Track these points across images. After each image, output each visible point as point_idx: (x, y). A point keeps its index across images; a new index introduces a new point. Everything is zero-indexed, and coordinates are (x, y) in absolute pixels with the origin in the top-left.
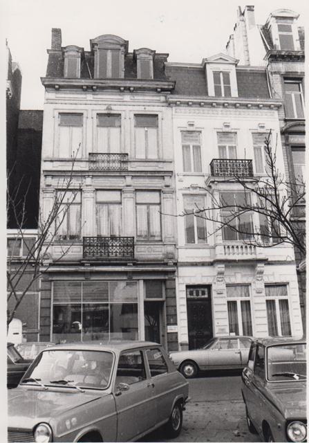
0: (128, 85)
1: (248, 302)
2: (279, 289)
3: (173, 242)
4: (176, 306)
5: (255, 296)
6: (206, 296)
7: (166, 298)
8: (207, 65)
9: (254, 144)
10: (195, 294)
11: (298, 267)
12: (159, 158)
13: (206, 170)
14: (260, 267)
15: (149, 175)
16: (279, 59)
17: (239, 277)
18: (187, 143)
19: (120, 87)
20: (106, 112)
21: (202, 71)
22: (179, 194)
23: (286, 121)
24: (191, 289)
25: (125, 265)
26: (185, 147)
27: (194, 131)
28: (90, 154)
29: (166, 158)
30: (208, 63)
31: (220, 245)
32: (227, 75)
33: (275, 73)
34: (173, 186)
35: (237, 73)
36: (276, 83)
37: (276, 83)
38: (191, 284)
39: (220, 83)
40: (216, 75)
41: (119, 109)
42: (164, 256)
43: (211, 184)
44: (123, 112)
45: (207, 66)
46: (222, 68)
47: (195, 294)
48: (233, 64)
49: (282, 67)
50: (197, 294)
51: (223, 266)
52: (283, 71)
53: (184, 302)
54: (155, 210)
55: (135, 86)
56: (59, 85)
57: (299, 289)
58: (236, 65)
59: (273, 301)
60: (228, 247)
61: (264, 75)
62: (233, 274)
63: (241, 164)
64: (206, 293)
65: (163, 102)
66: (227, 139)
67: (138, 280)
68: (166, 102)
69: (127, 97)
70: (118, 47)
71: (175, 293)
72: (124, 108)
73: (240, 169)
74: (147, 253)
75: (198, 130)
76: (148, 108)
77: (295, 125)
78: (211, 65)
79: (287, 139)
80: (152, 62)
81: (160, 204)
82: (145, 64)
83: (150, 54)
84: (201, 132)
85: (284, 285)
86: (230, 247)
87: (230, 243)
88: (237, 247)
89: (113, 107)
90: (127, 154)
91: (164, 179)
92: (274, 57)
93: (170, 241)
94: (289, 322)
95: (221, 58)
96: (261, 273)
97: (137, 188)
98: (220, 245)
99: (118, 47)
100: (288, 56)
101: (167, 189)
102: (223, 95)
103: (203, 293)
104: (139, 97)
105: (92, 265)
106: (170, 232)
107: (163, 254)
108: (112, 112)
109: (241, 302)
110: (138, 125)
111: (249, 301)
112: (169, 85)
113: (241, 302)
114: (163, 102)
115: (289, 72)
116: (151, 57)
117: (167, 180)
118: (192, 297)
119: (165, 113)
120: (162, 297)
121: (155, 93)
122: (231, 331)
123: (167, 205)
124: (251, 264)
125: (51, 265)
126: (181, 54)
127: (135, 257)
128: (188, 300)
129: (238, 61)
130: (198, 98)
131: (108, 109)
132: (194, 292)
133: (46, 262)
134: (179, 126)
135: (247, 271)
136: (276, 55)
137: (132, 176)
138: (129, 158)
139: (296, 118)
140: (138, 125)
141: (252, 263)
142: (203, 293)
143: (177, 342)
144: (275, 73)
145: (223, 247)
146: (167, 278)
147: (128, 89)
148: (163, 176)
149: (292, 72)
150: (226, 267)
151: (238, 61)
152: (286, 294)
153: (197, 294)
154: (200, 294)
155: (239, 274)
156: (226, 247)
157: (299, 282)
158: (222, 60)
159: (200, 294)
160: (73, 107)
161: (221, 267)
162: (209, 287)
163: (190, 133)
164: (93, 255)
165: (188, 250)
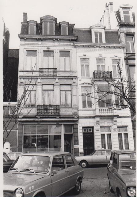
0: (57, 38)
1: (110, 134)
2: (124, 129)
3: (77, 107)
4: (78, 136)
5: (113, 132)
6: (91, 132)
7: (74, 132)
8: (92, 29)
9: (113, 64)
10: (86, 131)
11: (132, 119)
12: (71, 70)
13: (91, 75)
14: (115, 119)
15: (66, 78)
16: (124, 26)
17: (106, 123)
18: (83, 64)
19: (53, 39)
20: (47, 50)
21: (90, 32)
22: (79, 86)
23: (127, 54)
24: (85, 129)
25: (56, 118)
26: (82, 66)
27: (86, 58)
28: (40, 68)
29: (73, 70)
30: (92, 28)
31: (98, 109)
32: (100, 33)
33: (122, 32)
34: (77, 83)
35: (105, 32)
36: (123, 37)
37: (123, 37)
38: (85, 126)
39: (97, 37)
40: (96, 33)
41: (53, 49)
42: (73, 114)
43: (93, 82)
44: (55, 50)
45: (92, 29)
46: (99, 30)
47: (86, 131)
48: (103, 28)
49: (125, 30)
50: (88, 131)
51: (99, 118)
52: (125, 32)
53: (82, 134)
54: (69, 93)
55: (60, 38)
56: (26, 38)
57: (133, 128)
58: (105, 29)
59: (121, 134)
60: (101, 110)
61: (117, 33)
62: (103, 122)
63: (107, 73)
64: (92, 130)
65: (72, 45)
66: (101, 62)
67: (61, 124)
68: (74, 45)
69: (56, 43)
70: (52, 21)
71: (77, 130)
72: (55, 48)
73: (106, 75)
74: (65, 112)
75: (88, 58)
76: (65, 48)
77: (131, 56)
78: (94, 29)
79: (127, 62)
80: (67, 28)
81: (71, 91)
82: (64, 28)
83: (66, 24)
84: (89, 59)
85: (126, 127)
86: (102, 110)
87: (102, 108)
88: (105, 110)
89: (50, 48)
90: (56, 69)
91: (73, 79)
92: (122, 25)
93: (75, 107)
94: (128, 143)
95: (98, 26)
96: (116, 121)
97: (61, 84)
98: (98, 109)
99: (52, 21)
100: (128, 25)
101: (74, 84)
102: (99, 42)
103: (90, 130)
104: (62, 43)
105: (41, 118)
106: (75, 103)
107: (72, 113)
108: (50, 50)
109: (107, 134)
110: (61, 56)
111: (110, 134)
112: (75, 38)
113: (107, 134)
114: (72, 45)
115: (128, 32)
116: (67, 25)
117: (74, 80)
118: (85, 132)
119: (73, 50)
120: (72, 132)
121: (69, 41)
122: (102, 147)
123: (74, 91)
124: (111, 117)
125: (22, 118)
126: (80, 24)
127: (60, 114)
128: (83, 133)
129: (105, 27)
130: (88, 43)
131: (48, 48)
132: (86, 130)
133: (20, 117)
134: (79, 56)
135: (110, 121)
136: (122, 25)
137: (59, 78)
138: (57, 70)
139: (131, 52)
140: (61, 56)
141: (112, 117)
142: (90, 130)
143: (79, 152)
144: (122, 32)
145: (99, 110)
146: (74, 124)
147: (57, 40)
148: (72, 78)
149: (129, 32)
150: (100, 119)
151: (105, 27)
152: (127, 131)
153: (88, 131)
154: (89, 131)
155: (106, 122)
156: (100, 110)
157: (132, 125)
158: (98, 27)
159: (89, 131)
160: (32, 47)
161: (98, 119)
162: (93, 127)
163: (84, 59)
164: (41, 113)
165: (84, 111)
